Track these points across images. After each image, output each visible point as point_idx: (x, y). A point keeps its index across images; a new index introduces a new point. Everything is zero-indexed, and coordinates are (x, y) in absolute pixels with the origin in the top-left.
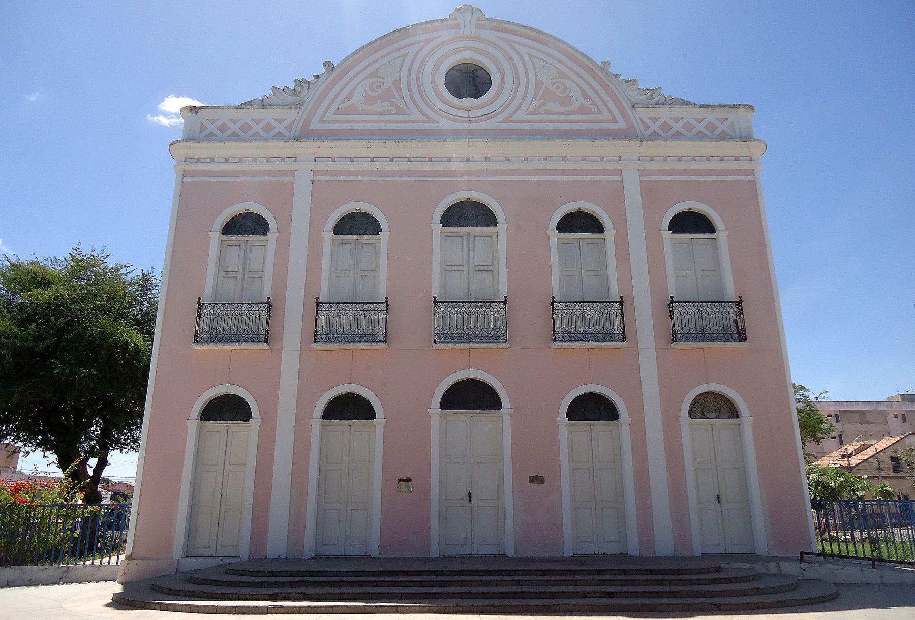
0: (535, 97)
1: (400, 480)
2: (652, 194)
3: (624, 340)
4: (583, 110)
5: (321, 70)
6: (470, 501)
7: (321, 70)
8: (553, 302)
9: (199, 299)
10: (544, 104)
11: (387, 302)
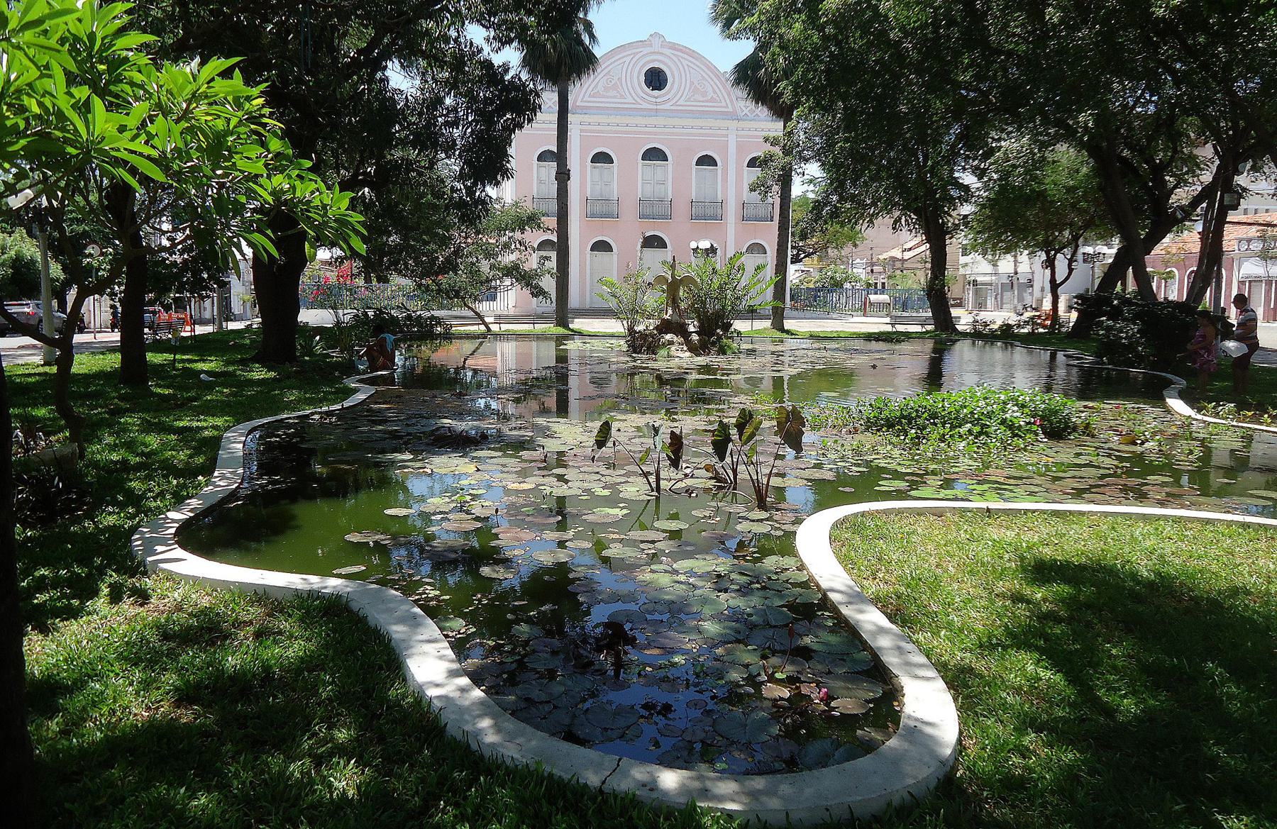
2: (741, 148)
4: (712, 100)
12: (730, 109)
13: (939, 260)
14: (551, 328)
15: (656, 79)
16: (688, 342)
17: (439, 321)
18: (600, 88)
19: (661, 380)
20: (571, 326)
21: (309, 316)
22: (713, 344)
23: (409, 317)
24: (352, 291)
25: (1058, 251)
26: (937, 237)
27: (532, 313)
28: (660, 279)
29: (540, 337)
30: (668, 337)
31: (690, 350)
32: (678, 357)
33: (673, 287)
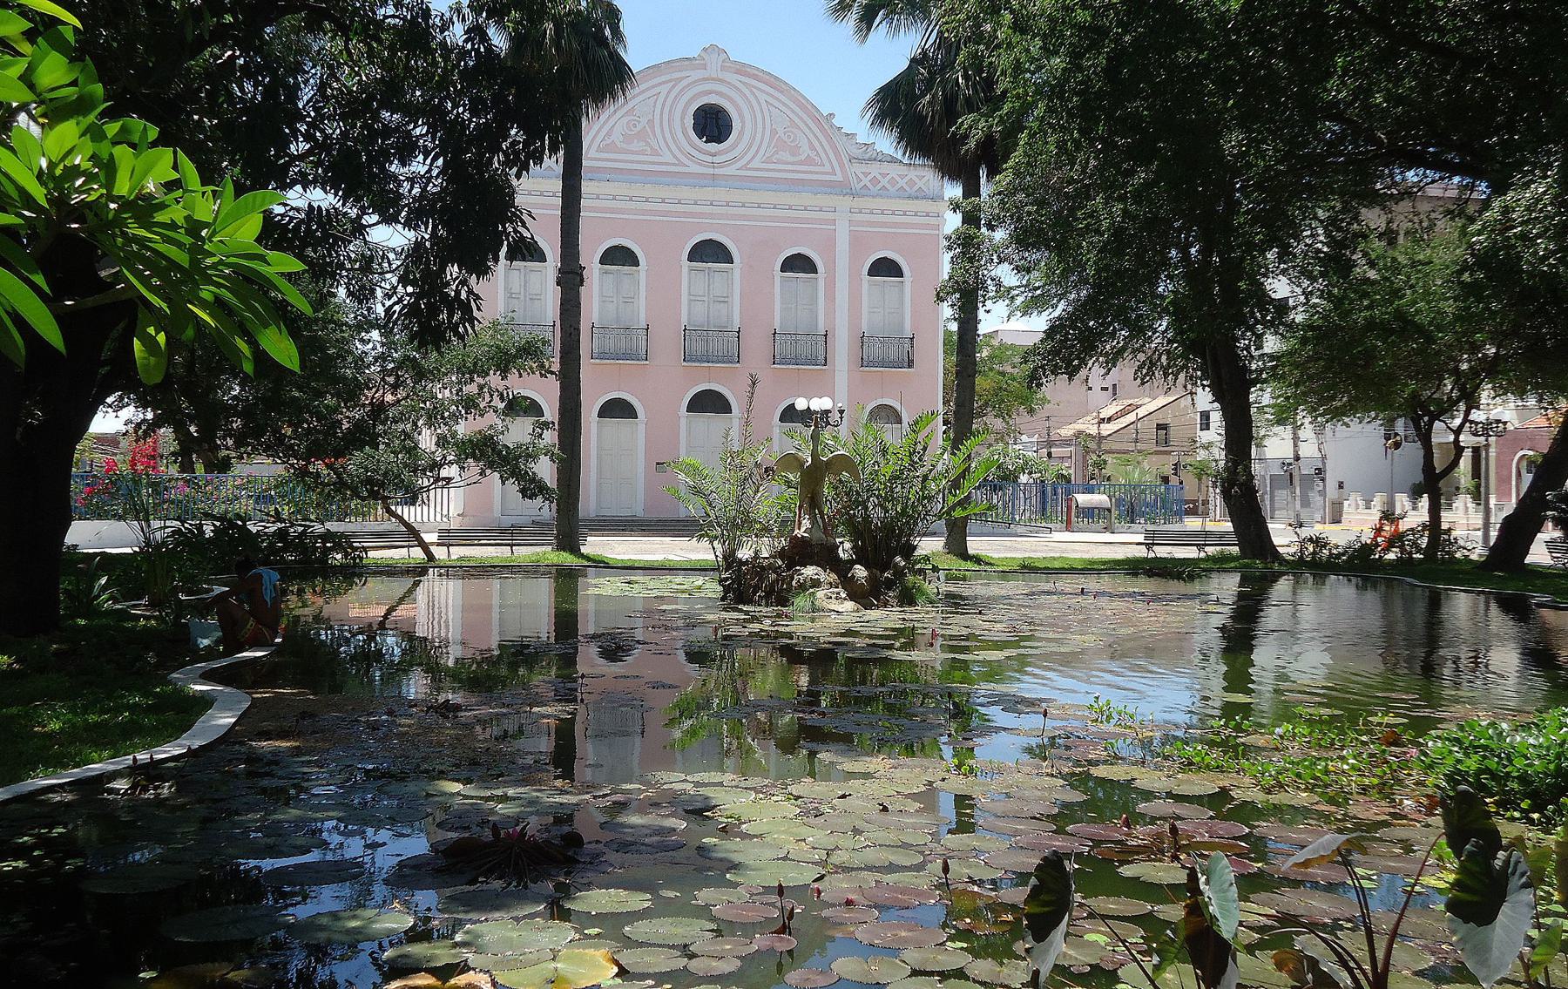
2: (857, 241)
4: (808, 161)
12: (839, 177)
13: (1240, 437)
14: (546, 553)
15: (712, 124)
16: (847, 582)
17: (341, 541)
18: (617, 137)
19: (792, 654)
20: (584, 550)
21: (84, 535)
22: (890, 584)
23: (282, 534)
24: (158, 487)
25: (1434, 417)
26: (1233, 393)
27: (494, 525)
28: (790, 461)
29: (532, 570)
30: (810, 571)
31: (852, 596)
32: (829, 612)
33: (812, 477)
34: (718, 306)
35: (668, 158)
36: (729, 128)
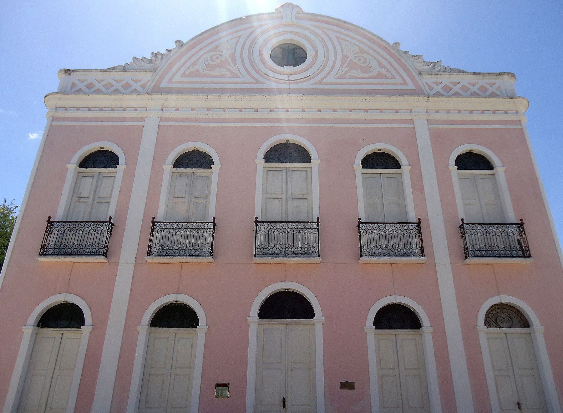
0: (342, 66)
1: (218, 385)
2: (439, 138)
3: (423, 256)
4: (379, 76)
5: (173, 46)
6: (284, 407)
7: (173, 46)
8: (360, 223)
9: (50, 218)
10: (349, 71)
11: (214, 222)
34: (296, 203)
35: (248, 79)
36: (456, 165)
